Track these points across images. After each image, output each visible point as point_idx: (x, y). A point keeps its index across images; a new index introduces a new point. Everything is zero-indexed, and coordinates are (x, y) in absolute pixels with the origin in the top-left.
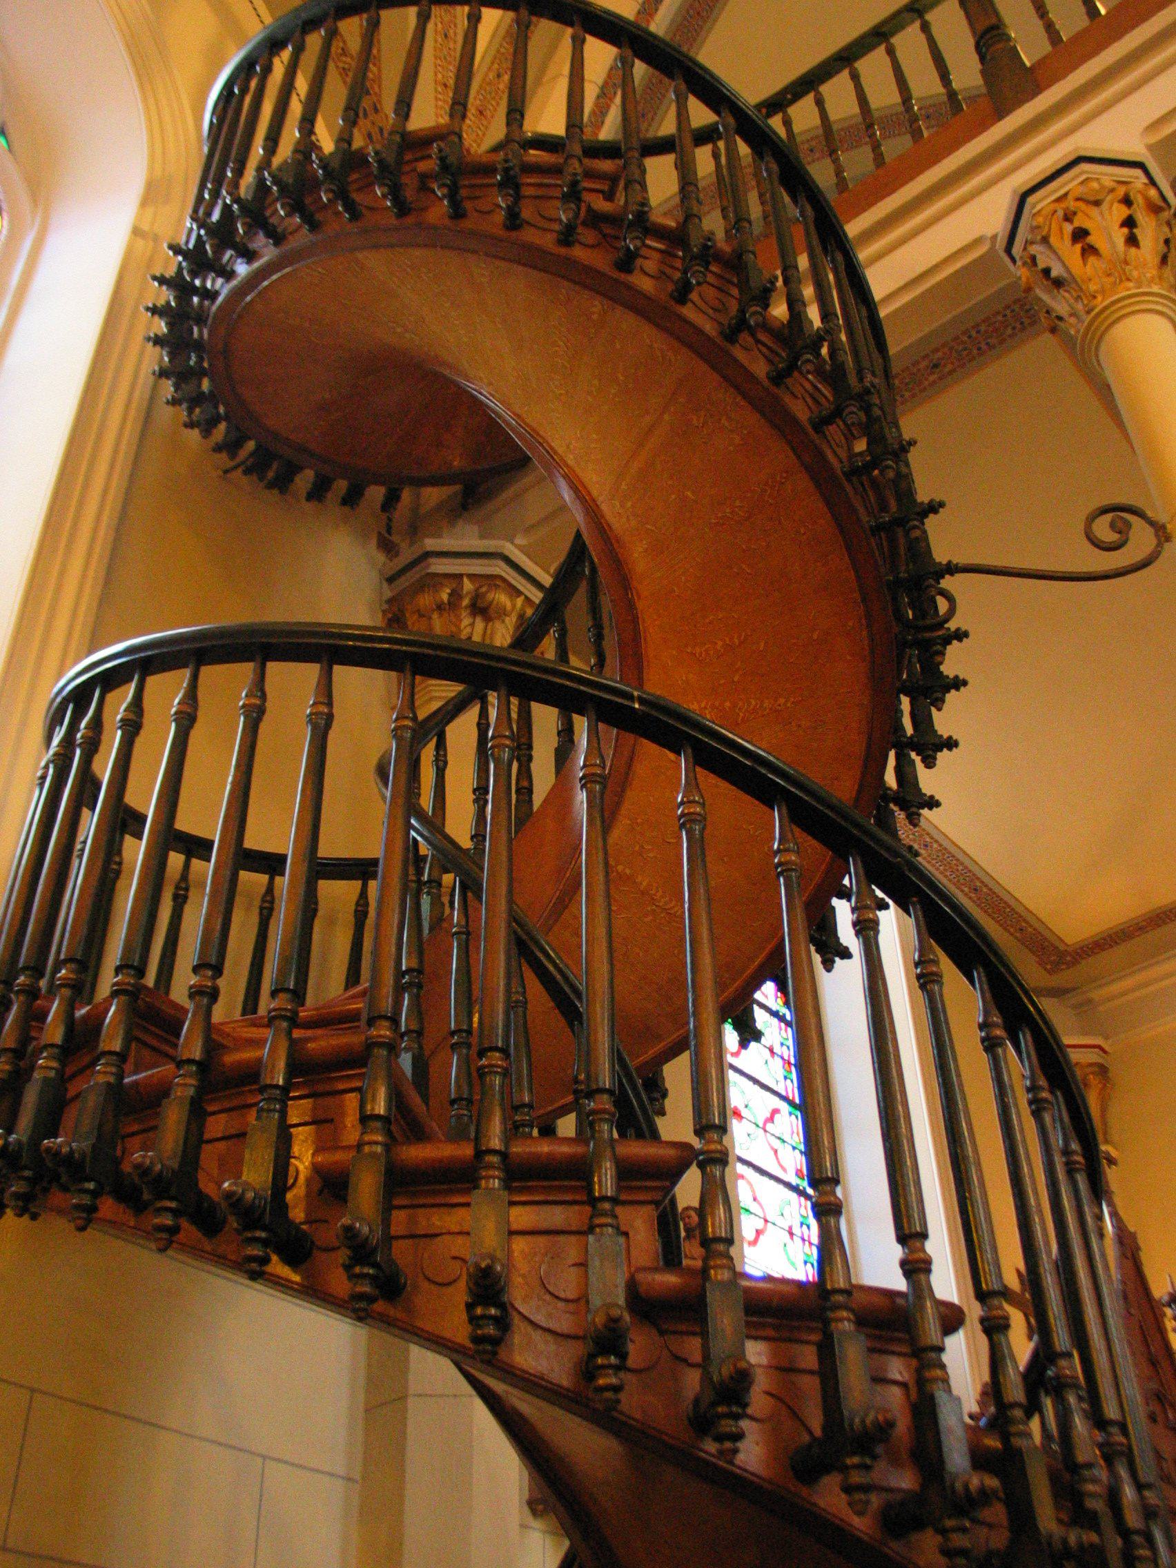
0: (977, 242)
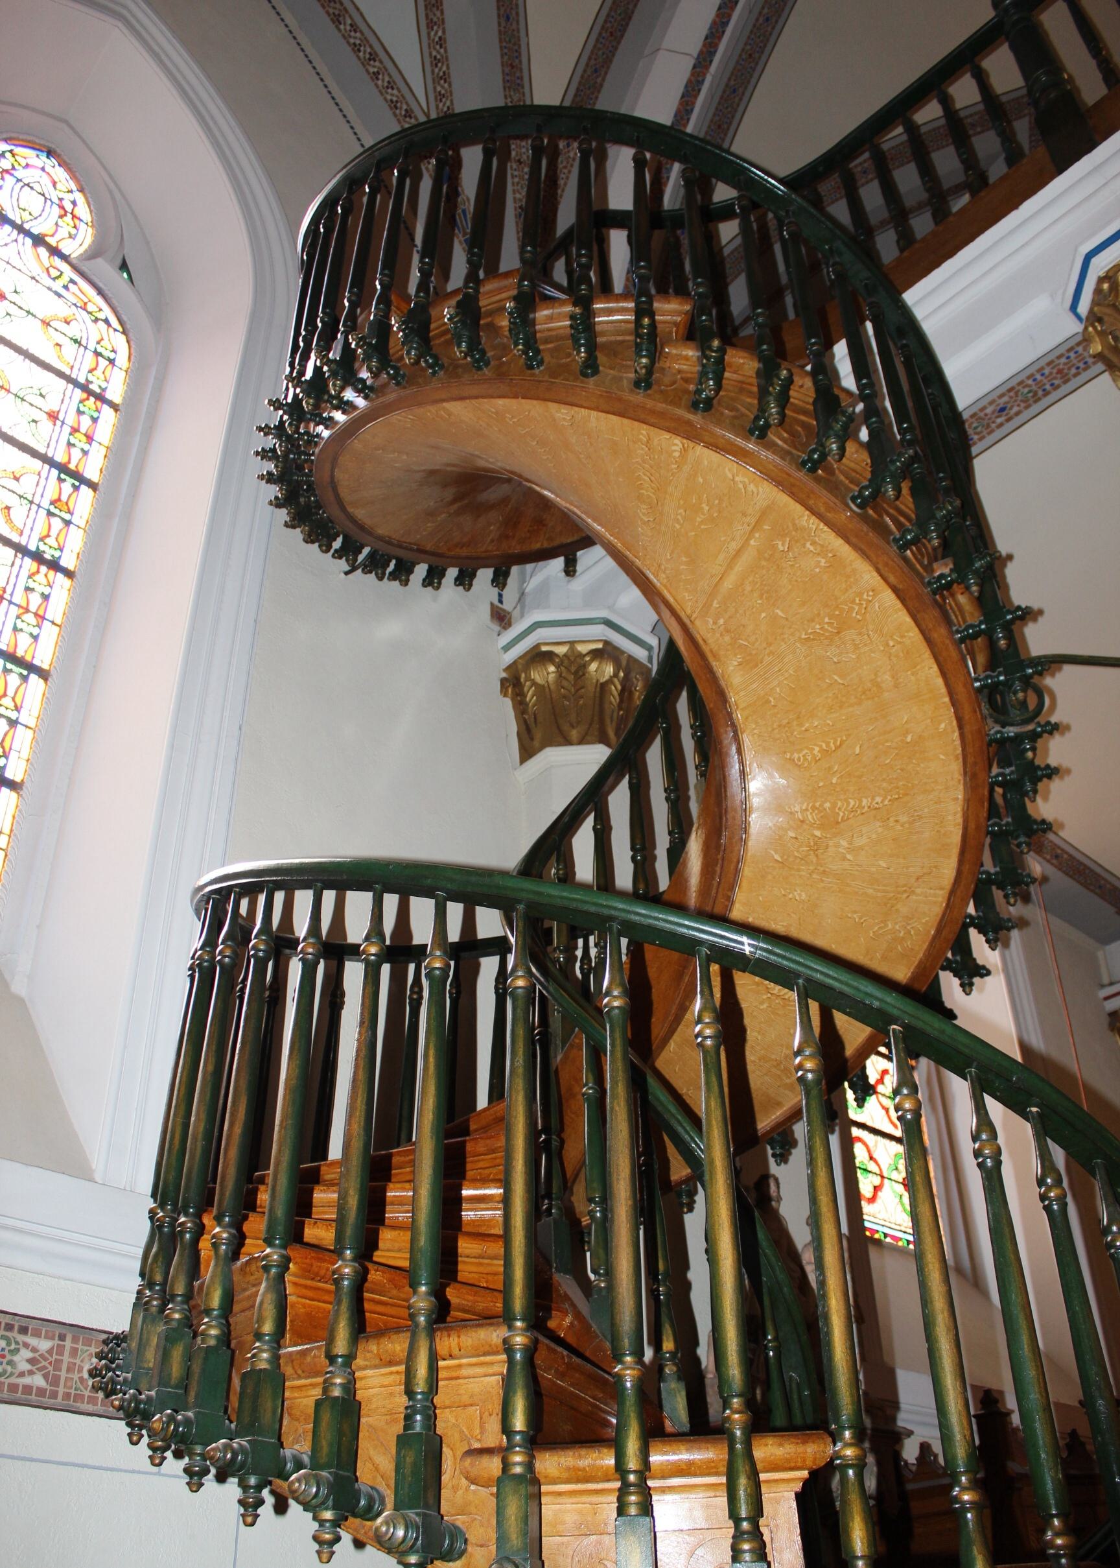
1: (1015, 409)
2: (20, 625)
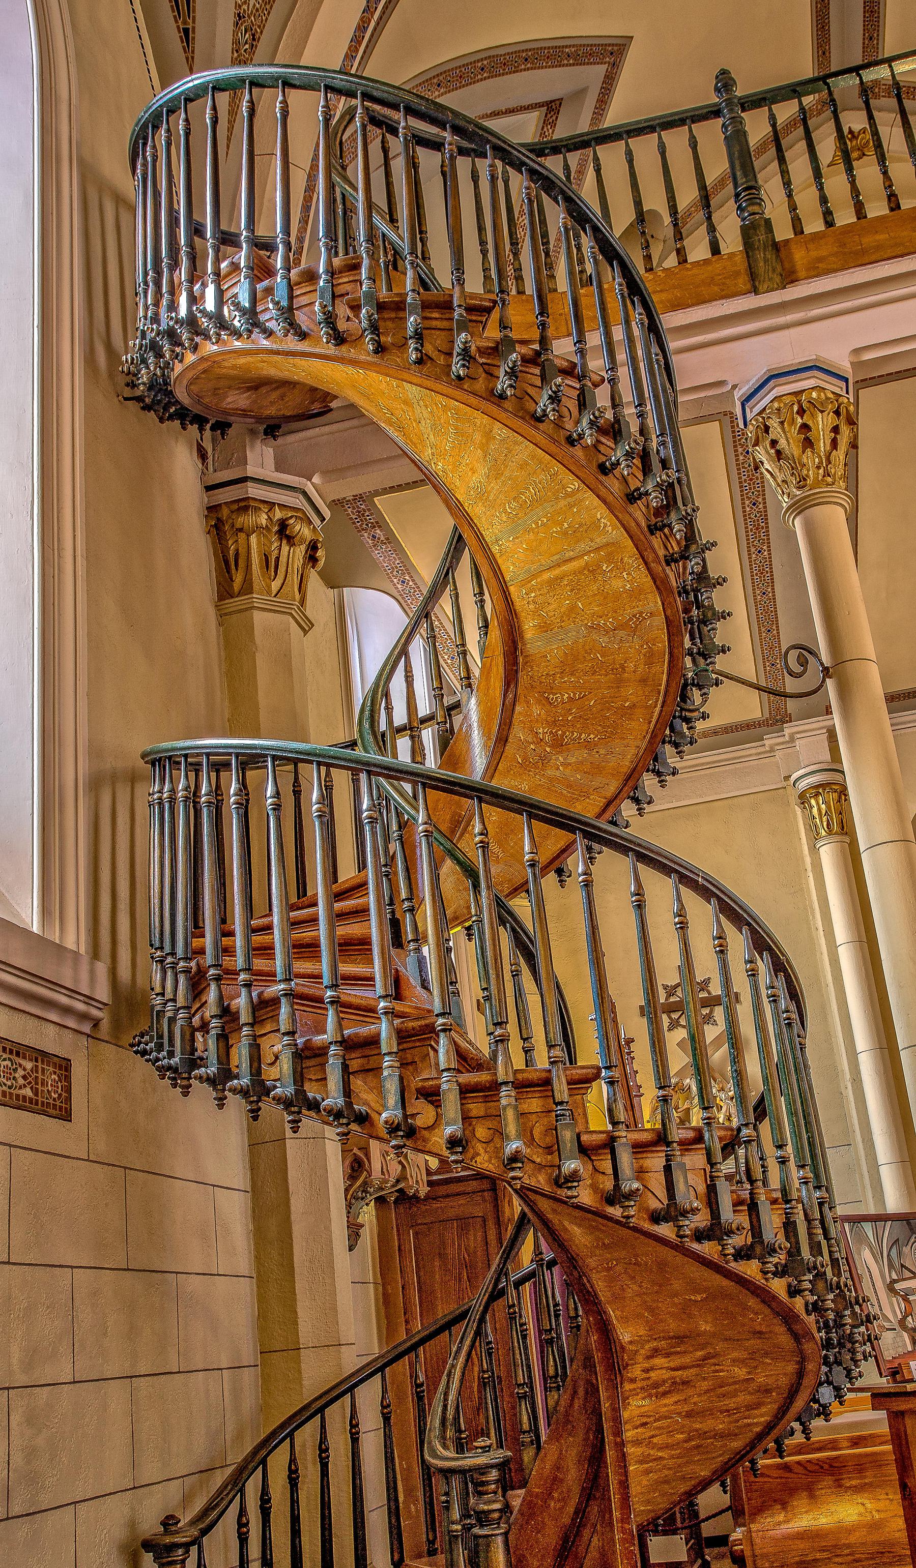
0: (721, 383)
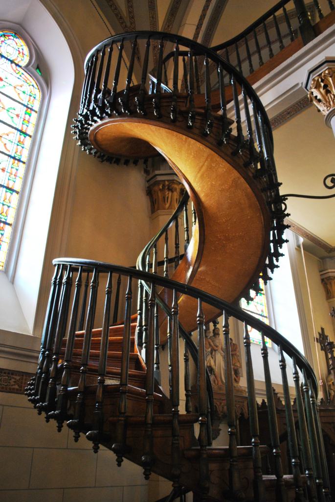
0: (298, 84)
1: (293, 113)
2: (10, 178)
